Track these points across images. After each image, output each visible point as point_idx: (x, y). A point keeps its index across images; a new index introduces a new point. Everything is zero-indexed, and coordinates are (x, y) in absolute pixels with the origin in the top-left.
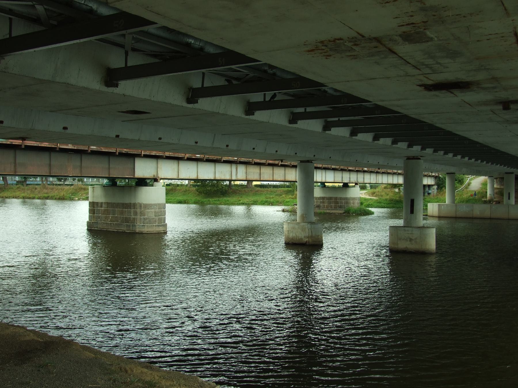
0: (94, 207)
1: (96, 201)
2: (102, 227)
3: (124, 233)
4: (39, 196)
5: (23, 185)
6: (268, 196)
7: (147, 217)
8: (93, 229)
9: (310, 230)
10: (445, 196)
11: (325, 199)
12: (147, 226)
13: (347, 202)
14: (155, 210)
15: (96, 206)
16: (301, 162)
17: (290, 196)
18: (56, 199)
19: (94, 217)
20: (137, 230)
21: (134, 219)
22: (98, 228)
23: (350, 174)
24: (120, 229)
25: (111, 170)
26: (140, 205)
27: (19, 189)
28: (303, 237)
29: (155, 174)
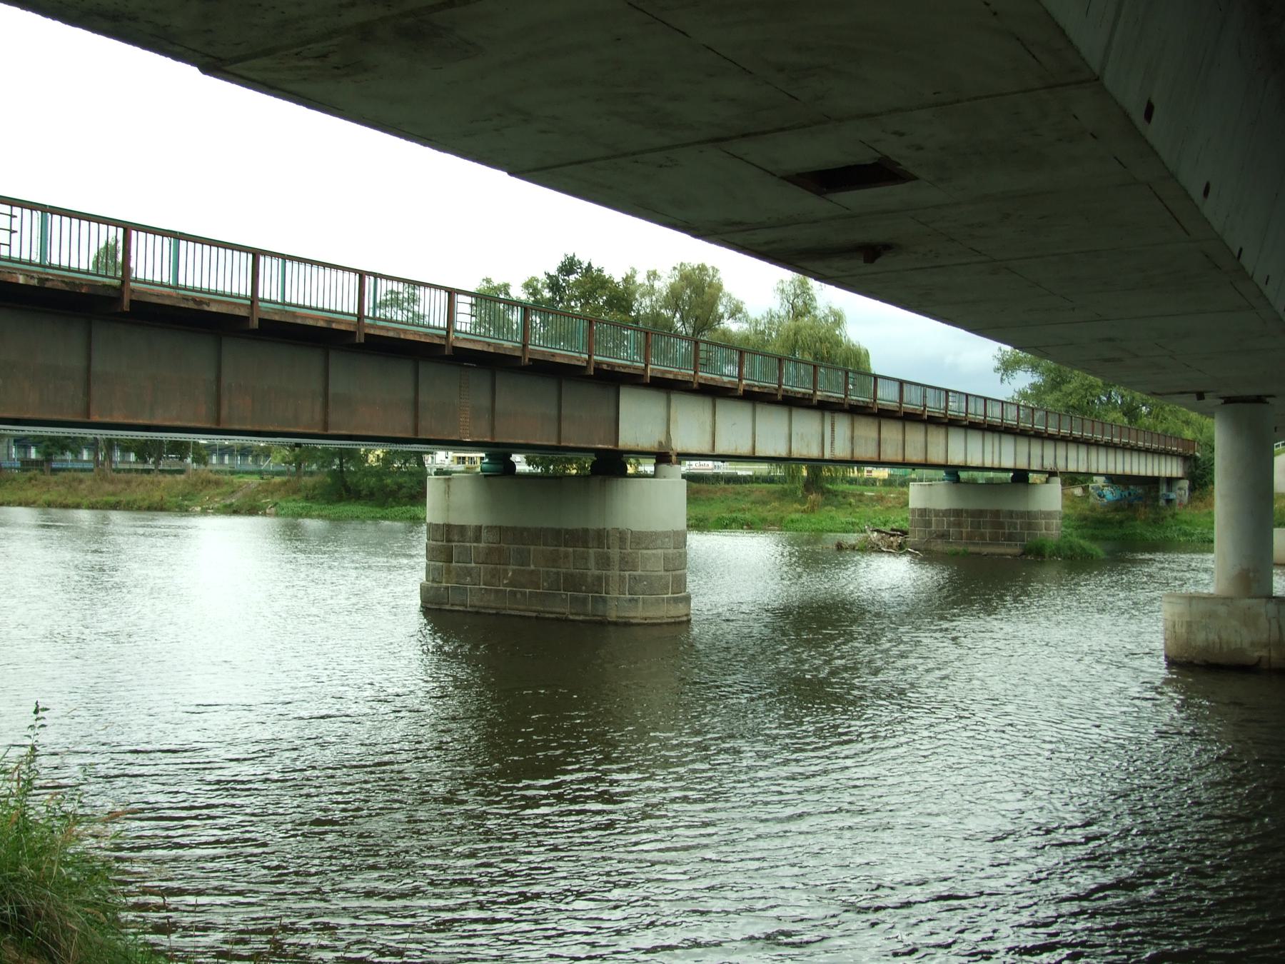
0: (449, 541)
1: (456, 520)
2: (482, 604)
3: (562, 621)
4: (94, 500)
5: (42, 470)
6: (735, 505)
7: (643, 573)
8: (447, 607)
9: (1274, 622)
10: (1211, 505)
11: (965, 515)
12: (644, 601)
13: (1030, 524)
14: (666, 551)
15: (456, 538)
16: (1225, 403)
17: (797, 506)
18: (139, 509)
19: (449, 571)
20: (613, 615)
21: (599, 578)
22: (586, 615)
23: (1030, 445)
24: (548, 609)
25: (564, 425)
26: (622, 536)
27: (33, 482)
28: (1246, 644)
29: (663, 440)
